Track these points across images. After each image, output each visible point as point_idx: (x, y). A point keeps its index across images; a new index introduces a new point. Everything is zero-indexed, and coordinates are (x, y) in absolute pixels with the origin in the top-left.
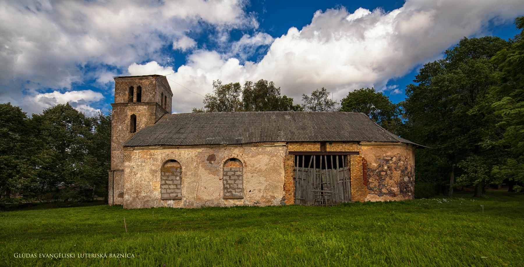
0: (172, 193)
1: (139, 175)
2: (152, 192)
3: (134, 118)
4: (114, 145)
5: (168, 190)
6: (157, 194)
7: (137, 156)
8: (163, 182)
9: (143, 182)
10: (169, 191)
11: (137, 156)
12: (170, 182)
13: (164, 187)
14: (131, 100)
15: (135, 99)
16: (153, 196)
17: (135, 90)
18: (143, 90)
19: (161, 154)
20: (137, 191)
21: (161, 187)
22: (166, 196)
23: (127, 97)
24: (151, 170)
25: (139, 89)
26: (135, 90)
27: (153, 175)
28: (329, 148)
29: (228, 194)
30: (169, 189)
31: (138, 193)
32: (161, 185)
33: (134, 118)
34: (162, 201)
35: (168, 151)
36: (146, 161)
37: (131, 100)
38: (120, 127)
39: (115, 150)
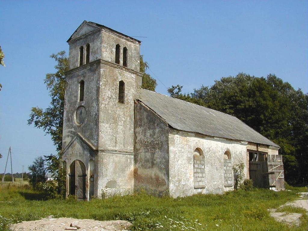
0: (200, 181)
1: (180, 162)
2: (188, 181)
3: (122, 84)
4: (102, 115)
5: (198, 178)
6: (191, 183)
7: (178, 141)
8: (195, 171)
9: (182, 170)
10: (199, 179)
11: (178, 141)
12: (199, 171)
13: (196, 175)
14: (117, 61)
15: (121, 62)
16: (189, 184)
17: (122, 51)
18: (129, 53)
19: (194, 141)
20: (179, 179)
21: (194, 176)
22: (197, 185)
23: (114, 56)
24: (188, 157)
25: (125, 50)
26: (122, 51)
27: (189, 163)
28: (261, 149)
29: (226, 183)
30: (199, 177)
31: (179, 181)
32: (194, 173)
33: (122, 84)
34: (195, 190)
35: (197, 139)
36: (184, 147)
37: (117, 61)
38: (109, 93)
39: (103, 122)
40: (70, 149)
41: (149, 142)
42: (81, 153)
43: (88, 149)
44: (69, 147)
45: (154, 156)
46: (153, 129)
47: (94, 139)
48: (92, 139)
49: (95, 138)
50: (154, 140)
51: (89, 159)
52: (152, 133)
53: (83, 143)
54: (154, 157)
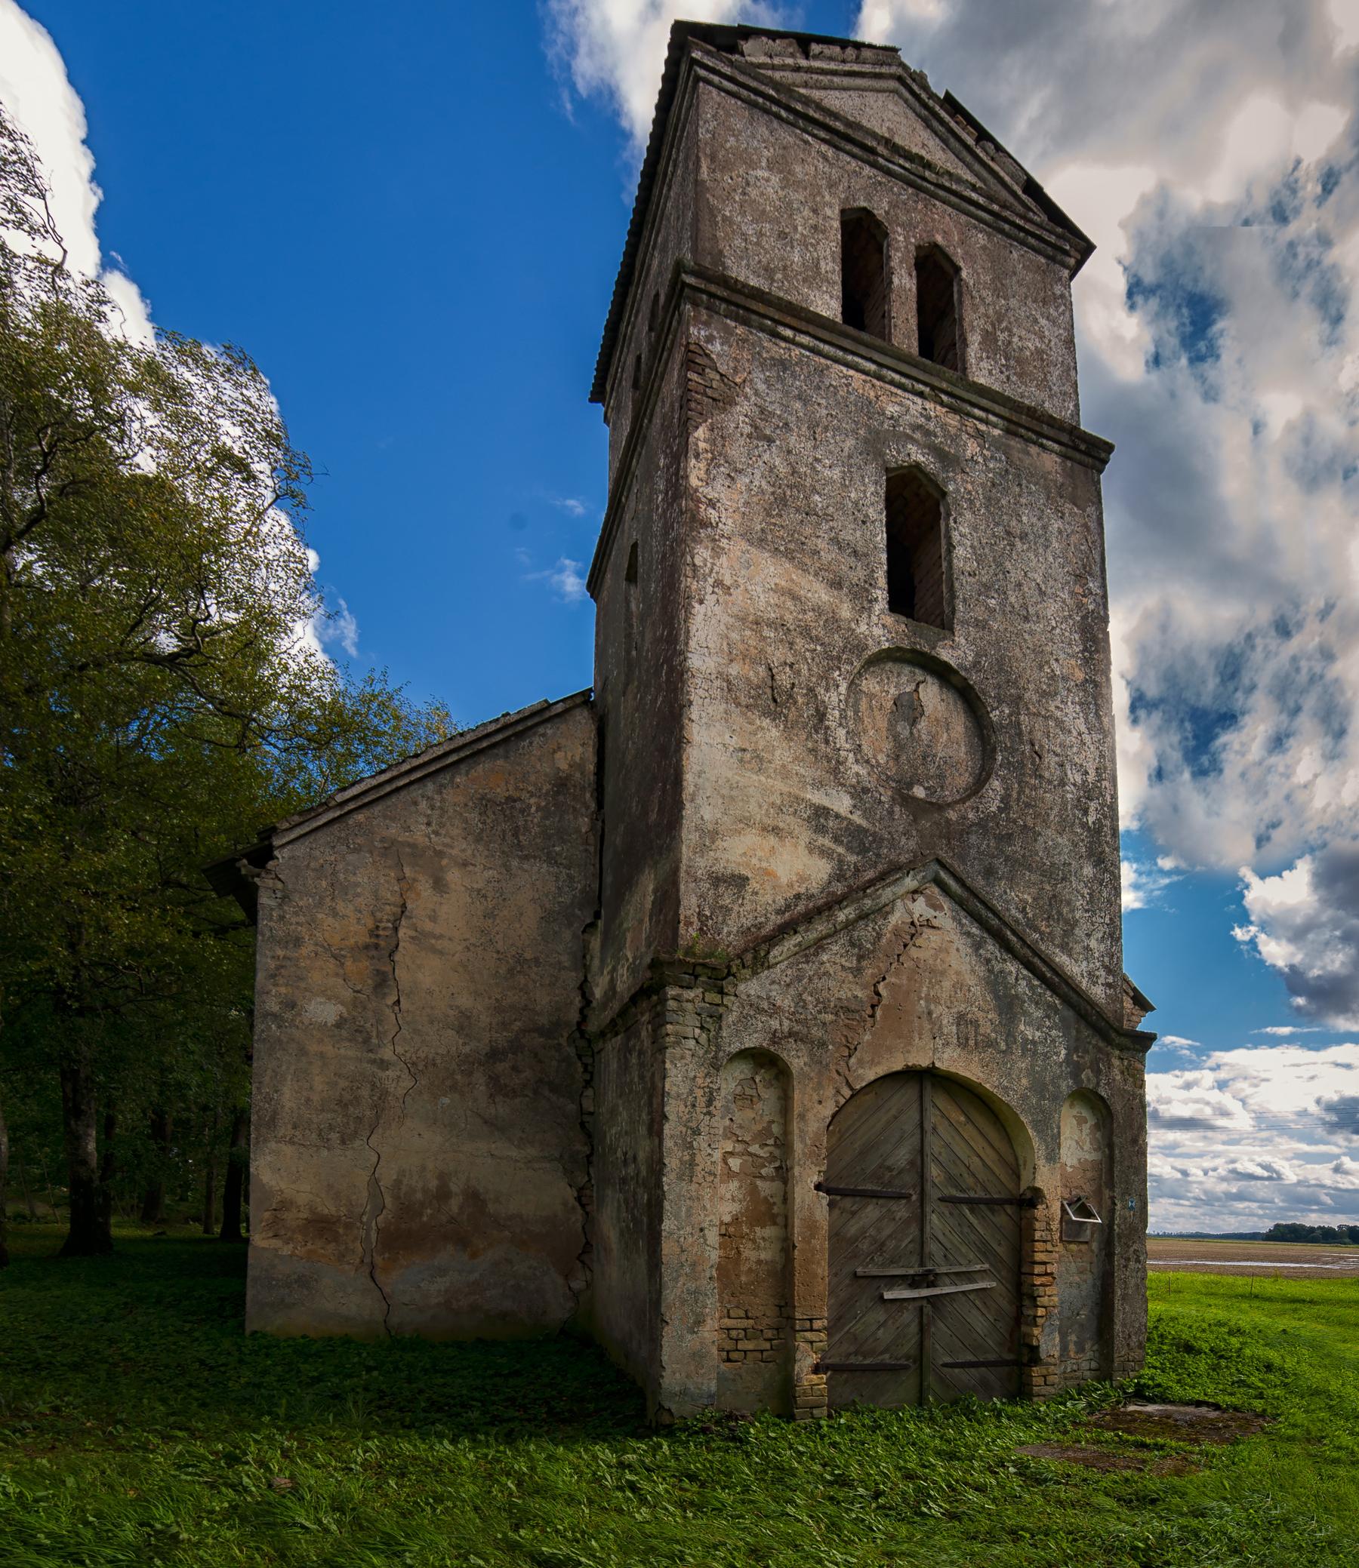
42: (975, 1024)
43: (1051, 1007)
47: (1078, 948)
48: (1065, 948)
49: (1087, 948)
53: (991, 948)
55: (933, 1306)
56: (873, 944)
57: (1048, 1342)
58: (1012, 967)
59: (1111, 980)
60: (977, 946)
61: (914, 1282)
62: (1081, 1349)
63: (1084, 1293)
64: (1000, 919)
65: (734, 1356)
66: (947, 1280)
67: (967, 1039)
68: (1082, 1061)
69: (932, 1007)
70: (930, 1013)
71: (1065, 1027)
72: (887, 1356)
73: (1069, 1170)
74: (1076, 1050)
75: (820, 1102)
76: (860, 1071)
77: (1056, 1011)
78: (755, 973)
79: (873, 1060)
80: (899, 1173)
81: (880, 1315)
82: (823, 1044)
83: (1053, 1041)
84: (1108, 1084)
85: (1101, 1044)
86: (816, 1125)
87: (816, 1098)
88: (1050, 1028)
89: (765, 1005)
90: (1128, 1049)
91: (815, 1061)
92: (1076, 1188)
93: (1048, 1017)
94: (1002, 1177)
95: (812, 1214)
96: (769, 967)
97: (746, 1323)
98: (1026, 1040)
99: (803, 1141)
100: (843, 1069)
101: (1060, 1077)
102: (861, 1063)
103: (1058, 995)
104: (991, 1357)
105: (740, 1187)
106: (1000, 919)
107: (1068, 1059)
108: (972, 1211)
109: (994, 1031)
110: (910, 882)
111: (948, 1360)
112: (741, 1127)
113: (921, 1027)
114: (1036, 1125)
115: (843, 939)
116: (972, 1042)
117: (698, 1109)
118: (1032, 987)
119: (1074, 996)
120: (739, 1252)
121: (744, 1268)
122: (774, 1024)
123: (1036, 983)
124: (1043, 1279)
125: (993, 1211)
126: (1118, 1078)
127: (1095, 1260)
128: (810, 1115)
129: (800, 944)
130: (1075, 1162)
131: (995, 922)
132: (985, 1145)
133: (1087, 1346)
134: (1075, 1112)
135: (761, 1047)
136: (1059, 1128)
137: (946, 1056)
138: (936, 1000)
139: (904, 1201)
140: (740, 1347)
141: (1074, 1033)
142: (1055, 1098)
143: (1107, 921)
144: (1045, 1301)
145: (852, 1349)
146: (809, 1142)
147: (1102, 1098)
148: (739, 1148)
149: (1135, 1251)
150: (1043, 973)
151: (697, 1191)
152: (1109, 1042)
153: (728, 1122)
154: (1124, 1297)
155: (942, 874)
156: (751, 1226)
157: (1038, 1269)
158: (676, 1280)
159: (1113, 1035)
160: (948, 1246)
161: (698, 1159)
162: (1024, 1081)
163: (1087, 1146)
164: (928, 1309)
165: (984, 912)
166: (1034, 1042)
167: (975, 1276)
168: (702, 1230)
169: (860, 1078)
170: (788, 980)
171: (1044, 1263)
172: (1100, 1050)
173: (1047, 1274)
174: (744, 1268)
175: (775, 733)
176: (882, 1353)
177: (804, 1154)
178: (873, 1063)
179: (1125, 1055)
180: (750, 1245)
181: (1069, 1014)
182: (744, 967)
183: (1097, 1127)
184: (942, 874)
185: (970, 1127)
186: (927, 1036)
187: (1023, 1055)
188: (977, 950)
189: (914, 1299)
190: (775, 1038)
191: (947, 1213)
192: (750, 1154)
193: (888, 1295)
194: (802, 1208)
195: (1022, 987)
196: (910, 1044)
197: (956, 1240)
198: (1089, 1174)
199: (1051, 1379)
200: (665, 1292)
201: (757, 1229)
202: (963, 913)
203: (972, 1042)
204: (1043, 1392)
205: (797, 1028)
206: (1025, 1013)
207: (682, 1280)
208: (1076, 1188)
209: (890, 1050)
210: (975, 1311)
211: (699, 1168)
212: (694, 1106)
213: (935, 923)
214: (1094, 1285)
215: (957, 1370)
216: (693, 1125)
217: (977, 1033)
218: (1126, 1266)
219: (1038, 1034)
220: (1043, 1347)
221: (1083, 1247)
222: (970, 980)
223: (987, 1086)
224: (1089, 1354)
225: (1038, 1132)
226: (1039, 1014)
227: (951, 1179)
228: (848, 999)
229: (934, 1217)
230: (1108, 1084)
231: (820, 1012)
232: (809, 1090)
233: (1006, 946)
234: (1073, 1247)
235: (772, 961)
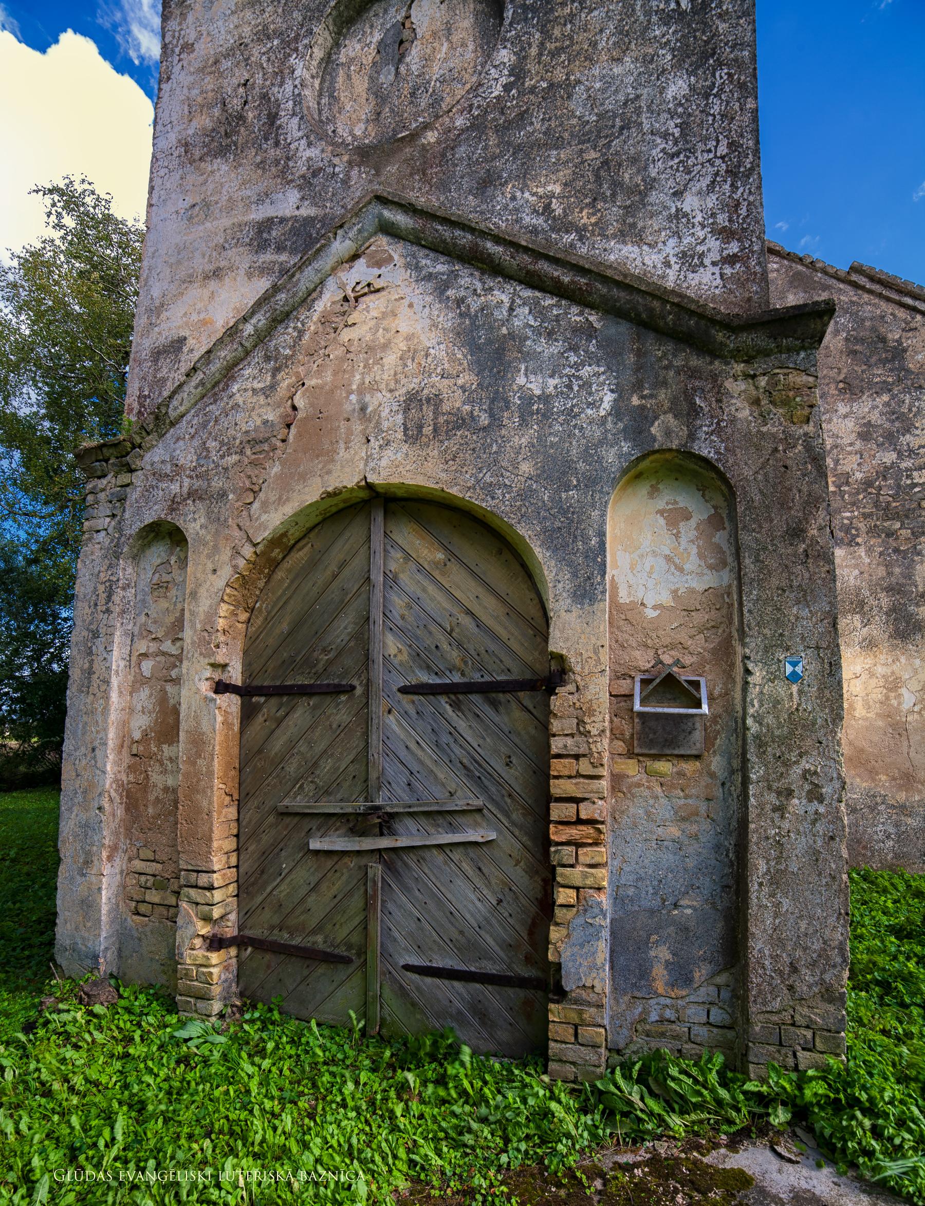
40: (251, 377)
41: (859, 475)
44: (229, 372)
45: (911, 566)
46: (885, 388)
50: (907, 464)
51: (613, 457)
52: (875, 417)
53: (468, 279)
54: (909, 576)
55: (390, 867)
56: (293, 347)
57: (585, 956)
58: (502, 295)
59: (734, 248)
60: (441, 288)
61: (357, 824)
62: (681, 975)
63: (691, 863)
64: (472, 230)
65: (143, 908)
66: (410, 823)
67: (420, 427)
68: (649, 403)
69: (368, 398)
70: (363, 409)
71: (611, 354)
72: (319, 939)
73: (651, 613)
74: (638, 386)
75: (215, 571)
76: (264, 517)
77: (589, 331)
78: (161, 436)
79: (280, 498)
80: (339, 654)
81: (304, 875)
82: (223, 495)
83: (586, 385)
84: (718, 431)
85: (695, 362)
86: (208, 602)
87: (210, 566)
88: (577, 366)
89: (168, 469)
90: (767, 353)
91: (216, 520)
92: (671, 647)
93: (574, 349)
94: (515, 646)
95: (198, 723)
96: (172, 424)
97: (155, 867)
98: (528, 399)
99: (193, 626)
100: (245, 523)
101: (601, 443)
102: (265, 506)
103: (591, 306)
104: (491, 968)
105: (151, 695)
106: (472, 230)
107: (617, 411)
108: (456, 706)
109: (470, 401)
110: (340, 246)
111: (414, 960)
112: (155, 622)
113: (350, 432)
114: (550, 537)
115: (259, 355)
116: (428, 430)
117: (99, 608)
118: (537, 310)
119: (623, 295)
120: (147, 777)
121: (152, 797)
122: (175, 488)
123: (549, 301)
124: (574, 832)
125: (495, 704)
126: (745, 413)
127: (718, 792)
128: (202, 592)
129: (202, 383)
130: (666, 598)
131: (465, 239)
132: (481, 591)
133: (700, 973)
134: (661, 504)
135: (160, 519)
136: (602, 534)
137: (384, 463)
138: (374, 387)
139: (343, 698)
140: (147, 898)
141: (631, 359)
142: (590, 483)
143: (723, 150)
144: (575, 875)
145: (276, 920)
146: (199, 626)
147: (705, 461)
148: (153, 647)
149: (805, 774)
150: (557, 282)
151: (92, 703)
152: (712, 351)
153: (143, 618)
154: (776, 880)
155: (387, 214)
156: (159, 744)
157: (568, 811)
158: (70, 810)
159: (720, 336)
160: (415, 767)
161: (96, 666)
162: (526, 468)
163: (692, 562)
164: (377, 870)
165: (446, 232)
166: (545, 398)
167: (461, 820)
168: (93, 750)
169: (263, 526)
170: (192, 431)
171: (577, 801)
172: (694, 373)
173: (579, 822)
174: (152, 797)
175: (225, 168)
176: (314, 932)
177: (193, 643)
178: (280, 501)
179: (758, 366)
180: (157, 767)
181: (621, 330)
182: (148, 434)
183: (715, 522)
184: (387, 214)
185: (453, 567)
186: (357, 439)
187: (524, 423)
188: (442, 292)
189: (359, 853)
190: (174, 505)
191: (412, 712)
192: (164, 654)
193: (315, 845)
194: (188, 716)
195: (524, 317)
196: (333, 461)
197: (427, 754)
198: (700, 618)
199: (587, 1032)
200: (62, 824)
201: (165, 747)
202: (422, 253)
203: (428, 430)
204: (571, 1056)
205: (197, 484)
206: (527, 356)
207: (75, 809)
208: (671, 647)
209: (303, 477)
210: (460, 882)
211: (96, 676)
212: (96, 605)
213: (378, 284)
214: (717, 847)
215: (429, 980)
216: (93, 627)
217: (436, 413)
218: (780, 810)
219: (552, 382)
220: (568, 967)
221: (689, 767)
222: (428, 339)
223: (454, 491)
224: (706, 992)
225: (555, 550)
226: (556, 348)
227: (420, 658)
228: (256, 429)
229: (391, 720)
230: (718, 431)
231: (223, 457)
232: (203, 557)
233: (492, 268)
234: (664, 766)
235: (173, 414)
